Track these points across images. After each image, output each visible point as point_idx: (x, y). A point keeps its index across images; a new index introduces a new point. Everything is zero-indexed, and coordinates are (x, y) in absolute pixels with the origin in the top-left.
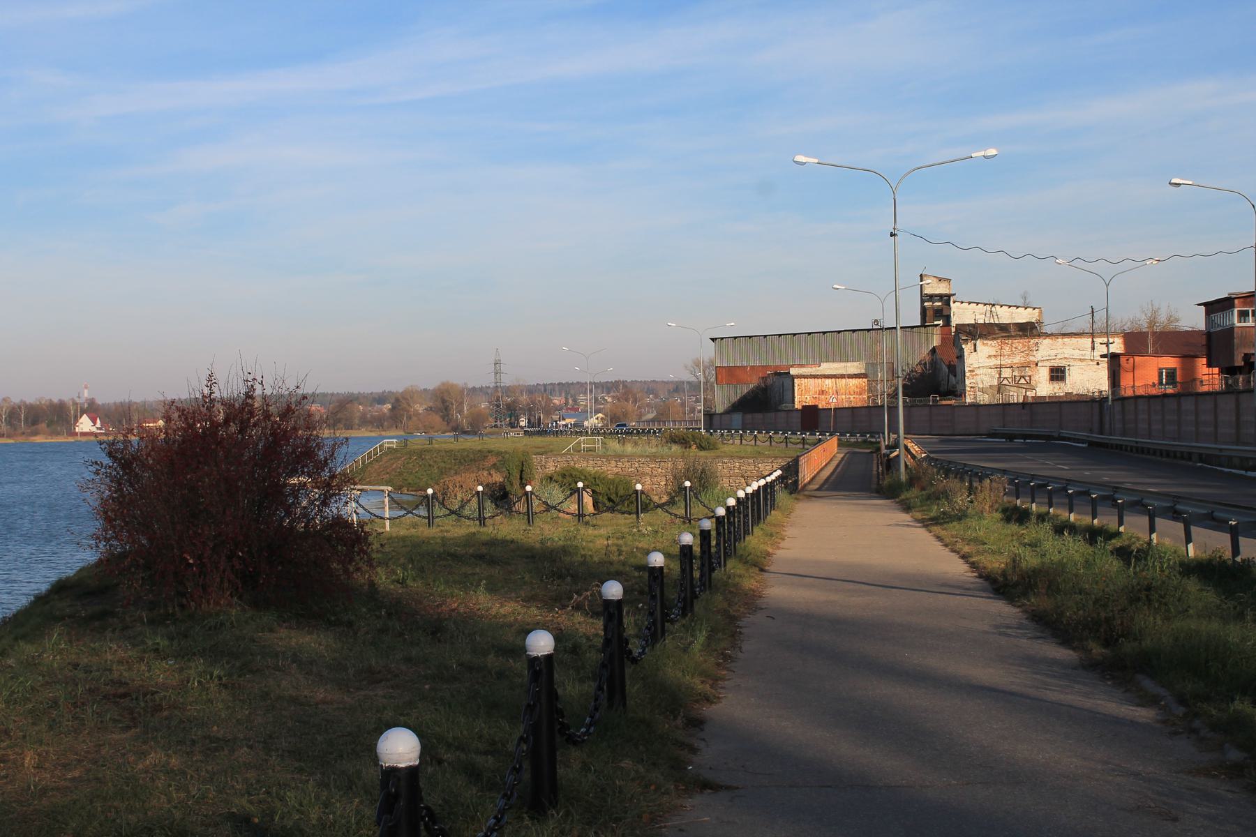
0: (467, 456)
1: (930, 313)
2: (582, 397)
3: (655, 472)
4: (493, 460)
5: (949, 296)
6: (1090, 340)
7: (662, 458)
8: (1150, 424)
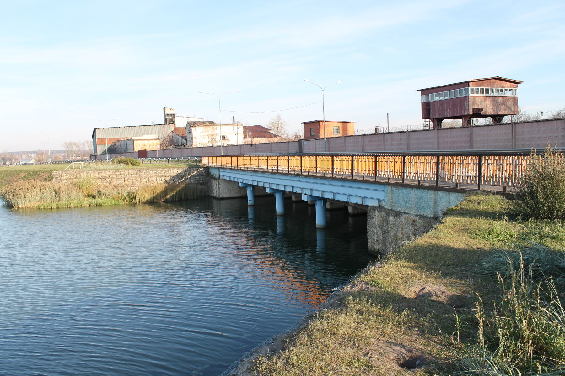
0: (9, 173)
1: (168, 120)
2: (23, 155)
3: (118, 177)
4: (23, 175)
5: (174, 115)
6: (233, 127)
7: (121, 170)
8: (345, 146)
